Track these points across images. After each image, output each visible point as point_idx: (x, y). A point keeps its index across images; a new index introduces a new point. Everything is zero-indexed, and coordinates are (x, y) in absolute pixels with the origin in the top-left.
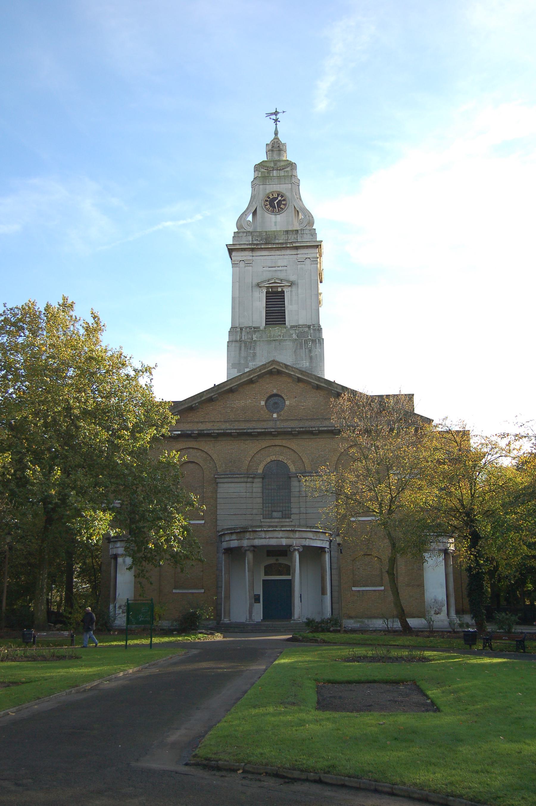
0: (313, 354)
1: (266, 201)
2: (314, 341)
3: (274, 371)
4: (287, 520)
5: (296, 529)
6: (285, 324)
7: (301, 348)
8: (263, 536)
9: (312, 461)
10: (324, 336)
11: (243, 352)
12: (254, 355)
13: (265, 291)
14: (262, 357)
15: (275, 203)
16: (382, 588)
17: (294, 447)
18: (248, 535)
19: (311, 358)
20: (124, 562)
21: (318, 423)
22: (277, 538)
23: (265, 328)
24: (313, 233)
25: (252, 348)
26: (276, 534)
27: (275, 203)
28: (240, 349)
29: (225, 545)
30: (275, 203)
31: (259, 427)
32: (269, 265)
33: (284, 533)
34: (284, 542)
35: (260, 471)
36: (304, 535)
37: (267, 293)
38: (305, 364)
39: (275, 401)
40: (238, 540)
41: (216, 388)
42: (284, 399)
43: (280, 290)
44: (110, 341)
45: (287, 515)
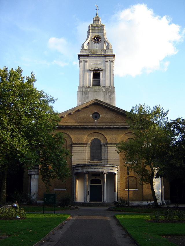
0: (111, 97)
1: (98, 37)
2: (111, 92)
3: (97, 104)
4: (100, 162)
5: (105, 165)
6: (100, 85)
7: (106, 95)
8: (92, 168)
9: (110, 139)
10: (116, 90)
11: (83, 95)
12: (88, 97)
14: (91, 99)
15: (98, 39)
16: (66, 189)
17: (103, 133)
18: (86, 168)
19: (110, 99)
20: (34, 177)
21: (113, 124)
22: (98, 169)
23: (92, 87)
24: (112, 51)
25: (87, 94)
26: (97, 167)
27: (97, 39)
28: (82, 94)
29: (76, 171)
30: (98, 39)
31: (90, 125)
32: (92, 63)
33: (100, 167)
34: (100, 170)
36: (108, 168)
38: (107, 101)
39: (96, 116)
40: (82, 169)
41: (73, 109)
42: (99, 114)
43: (98, 72)
44: (38, 86)
45: (100, 160)
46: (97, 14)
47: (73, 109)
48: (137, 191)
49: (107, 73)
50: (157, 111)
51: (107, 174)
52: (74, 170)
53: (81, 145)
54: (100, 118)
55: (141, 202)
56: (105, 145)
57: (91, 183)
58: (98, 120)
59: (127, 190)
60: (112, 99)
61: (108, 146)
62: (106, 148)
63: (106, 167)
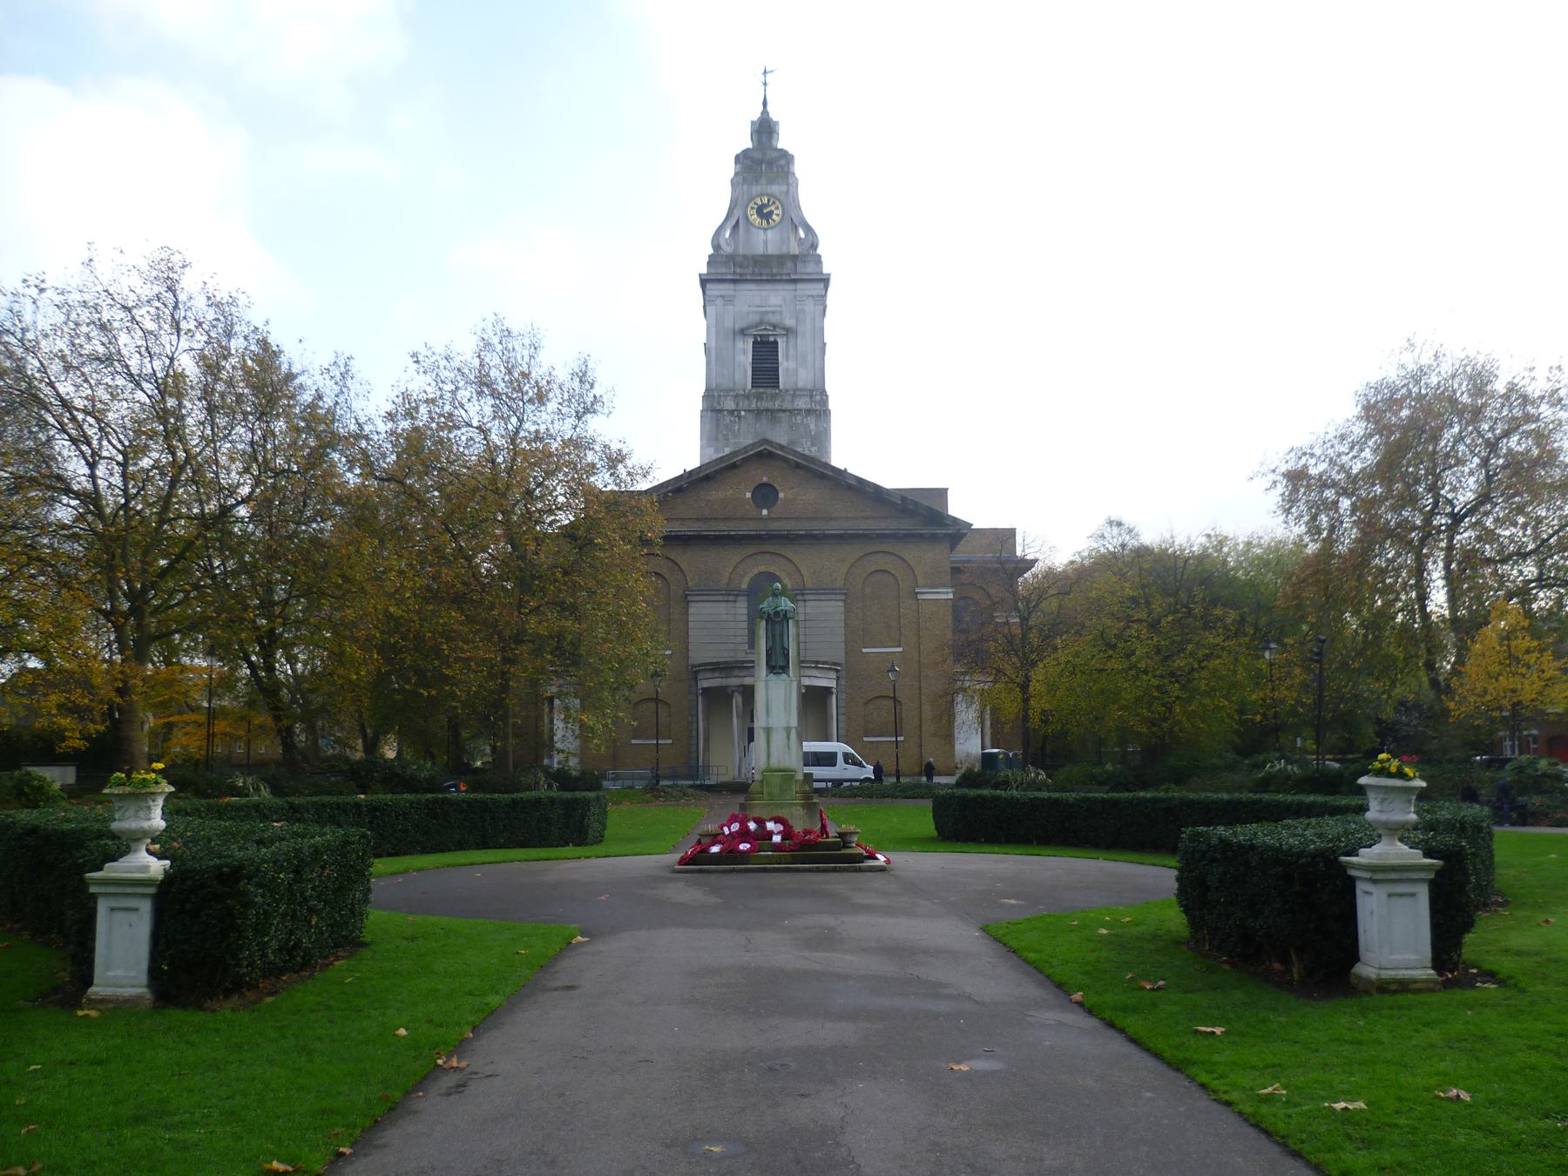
3: (765, 455)
13: (751, 340)
14: (745, 437)
17: (789, 554)
18: (736, 672)
32: (756, 301)
35: (744, 586)
38: (813, 451)
46: (765, 104)
47: (688, 475)
49: (803, 343)
59: (936, 779)
60: (822, 438)
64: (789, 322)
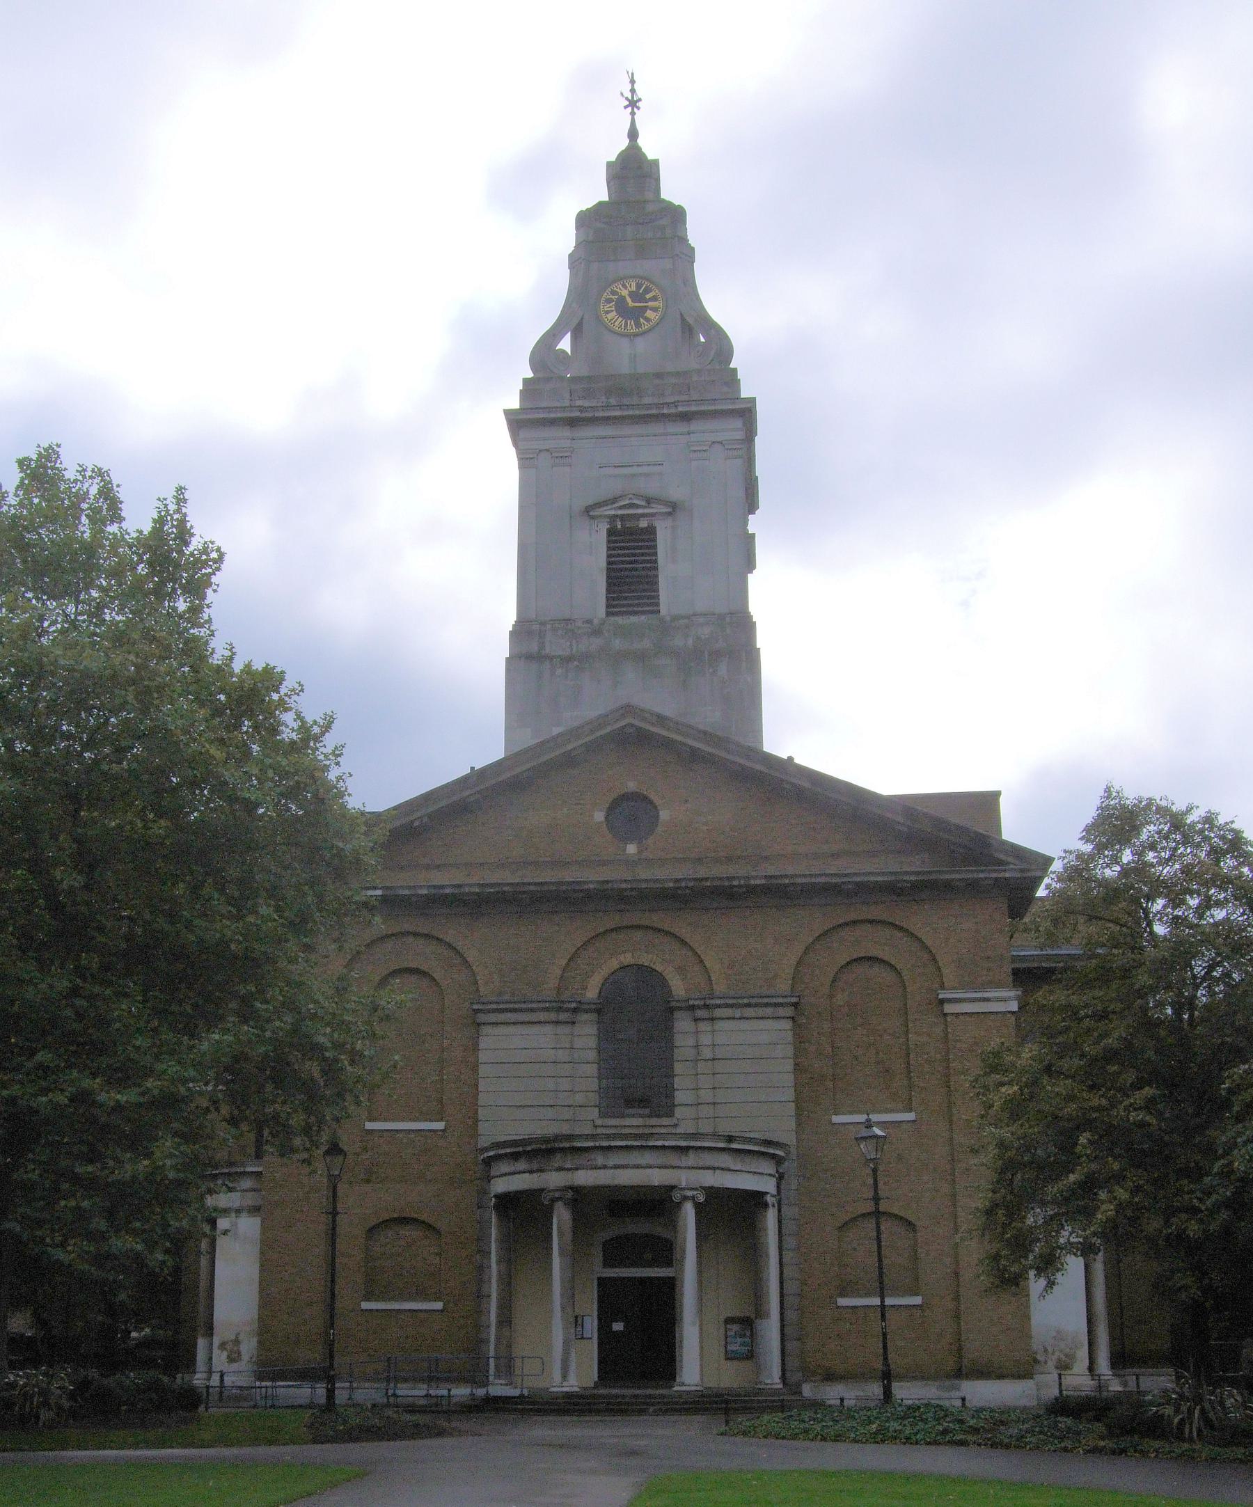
3: (635, 738)
13: (604, 528)
14: (594, 700)
18: (557, 1161)
24: (732, 379)
34: (657, 1178)
37: (611, 532)
39: (632, 813)
40: (531, 1172)
42: (651, 802)
43: (643, 524)
48: (918, 1313)
50: (274, 668)
51: (701, 1199)
52: (489, 1179)
53: (521, 1010)
54: (659, 829)
55: (947, 1383)
56: (693, 1008)
57: (607, 1264)
58: (650, 841)
61: (718, 1013)
62: (704, 1026)
63: (691, 1154)
64: (676, 493)
